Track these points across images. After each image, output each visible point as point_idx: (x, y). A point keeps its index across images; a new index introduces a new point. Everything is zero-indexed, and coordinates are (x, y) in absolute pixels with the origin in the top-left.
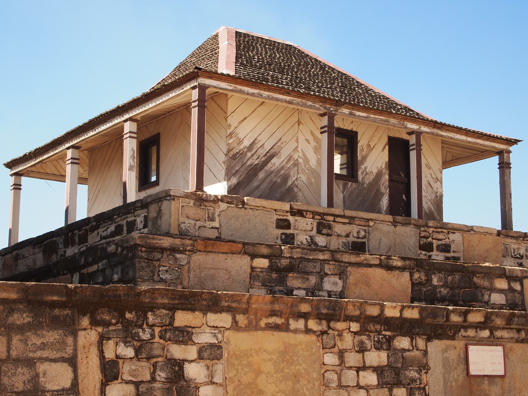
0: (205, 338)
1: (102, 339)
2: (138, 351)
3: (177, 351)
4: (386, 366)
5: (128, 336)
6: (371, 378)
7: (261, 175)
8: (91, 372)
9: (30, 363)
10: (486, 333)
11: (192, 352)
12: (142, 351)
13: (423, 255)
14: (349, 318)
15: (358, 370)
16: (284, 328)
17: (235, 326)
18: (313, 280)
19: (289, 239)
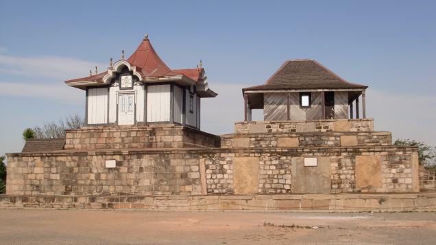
0: (228, 159)
1: (205, 160)
2: (213, 163)
3: (222, 162)
4: (134, 126)
5: (211, 158)
6: (274, 168)
7: (276, 111)
8: (203, 167)
9: (190, 166)
10: (311, 154)
11: (225, 163)
12: (214, 163)
13: (318, 130)
14: (267, 153)
15: (270, 165)
16: (249, 156)
17: (236, 156)
18: (268, 142)
19: (270, 131)
